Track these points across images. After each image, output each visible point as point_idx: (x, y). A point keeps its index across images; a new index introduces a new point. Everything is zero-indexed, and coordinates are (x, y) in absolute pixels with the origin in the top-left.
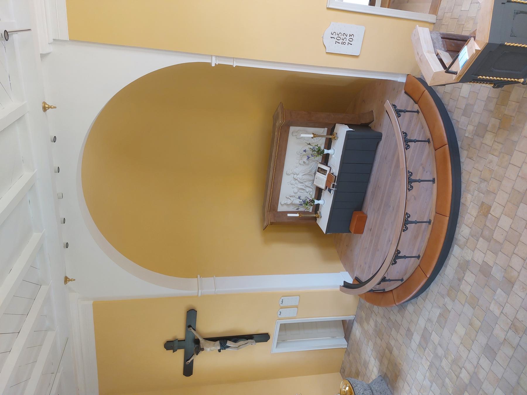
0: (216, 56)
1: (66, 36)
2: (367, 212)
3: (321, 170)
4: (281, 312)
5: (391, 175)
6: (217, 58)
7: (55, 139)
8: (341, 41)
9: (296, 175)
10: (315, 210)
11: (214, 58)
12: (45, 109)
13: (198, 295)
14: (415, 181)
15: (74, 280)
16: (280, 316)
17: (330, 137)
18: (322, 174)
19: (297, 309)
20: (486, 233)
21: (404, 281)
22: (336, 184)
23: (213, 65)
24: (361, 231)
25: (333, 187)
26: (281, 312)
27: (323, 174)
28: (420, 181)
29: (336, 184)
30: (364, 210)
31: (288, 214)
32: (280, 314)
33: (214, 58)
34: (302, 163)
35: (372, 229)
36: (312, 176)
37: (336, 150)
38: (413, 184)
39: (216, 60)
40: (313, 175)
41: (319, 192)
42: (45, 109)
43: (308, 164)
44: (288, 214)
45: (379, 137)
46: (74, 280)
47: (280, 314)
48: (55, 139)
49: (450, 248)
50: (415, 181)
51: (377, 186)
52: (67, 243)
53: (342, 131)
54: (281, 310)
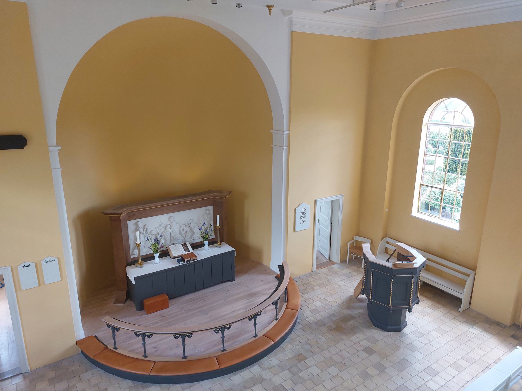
0: (289, 134)
1: (295, 29)
2: (171, 305)
3: (186, 246)
4: (30, 265)
5: (226, 301)
6: (288, 135)
7: (239, 6)
8: (302, 215)
9: (170, 226)
10: (148, 257)
11: (288, 132)
12: (269, 7)
13: (49, 147)
14: (183, 341)
15: (270, 15)
16: (20, 268)
17: (140, 260)
18: (184, 249)
19: (38, 286)
20: (295, 369)
21: (278, 319)
22: (191, 262)
23: (59, 148)
24: (151, 311)
25: (187, 261)
26: (30, 265)
27: (185, 250)
28: (184, 345)
29: (191, 262)
30: (171, 302)
31: (219, 216)
32: (24, 266)
33: (288, 132)
34: (182, 228)
35: (166, 317)
36: (170, 243)
37: (209, 251)
38: (180, 339)
39: (286, 134)
40: (172, 243)
41: (165, 254)
42: (269, 7)
43: (180, 234)
44: (219, 216)
45: (232, 279)
46: (270, 15)
47: (24, 266)
48: (239, 6)
49: (251, 365)
50: (183, 341)
51: (203, 298)
52: (241, 7)
53: (226, 248)
54: (33, 265)
